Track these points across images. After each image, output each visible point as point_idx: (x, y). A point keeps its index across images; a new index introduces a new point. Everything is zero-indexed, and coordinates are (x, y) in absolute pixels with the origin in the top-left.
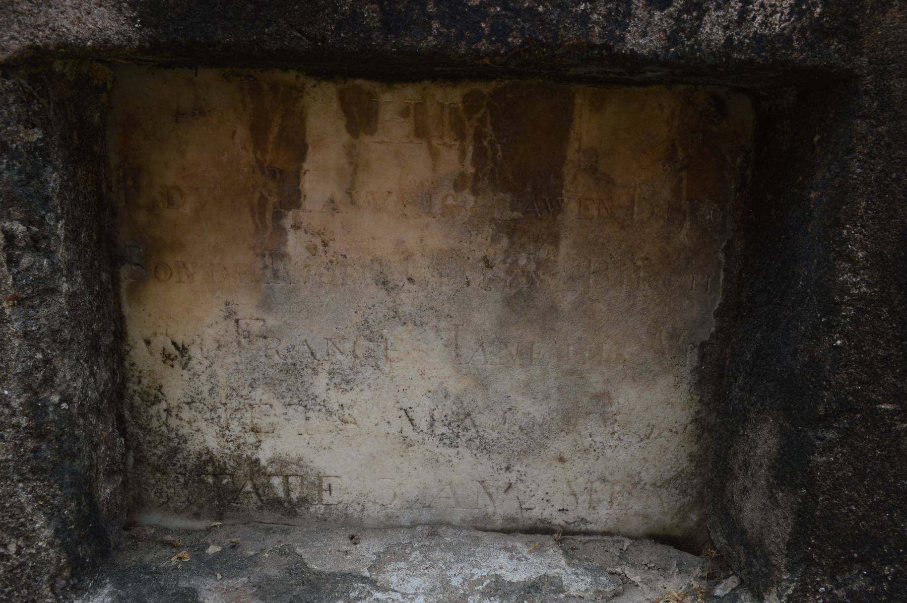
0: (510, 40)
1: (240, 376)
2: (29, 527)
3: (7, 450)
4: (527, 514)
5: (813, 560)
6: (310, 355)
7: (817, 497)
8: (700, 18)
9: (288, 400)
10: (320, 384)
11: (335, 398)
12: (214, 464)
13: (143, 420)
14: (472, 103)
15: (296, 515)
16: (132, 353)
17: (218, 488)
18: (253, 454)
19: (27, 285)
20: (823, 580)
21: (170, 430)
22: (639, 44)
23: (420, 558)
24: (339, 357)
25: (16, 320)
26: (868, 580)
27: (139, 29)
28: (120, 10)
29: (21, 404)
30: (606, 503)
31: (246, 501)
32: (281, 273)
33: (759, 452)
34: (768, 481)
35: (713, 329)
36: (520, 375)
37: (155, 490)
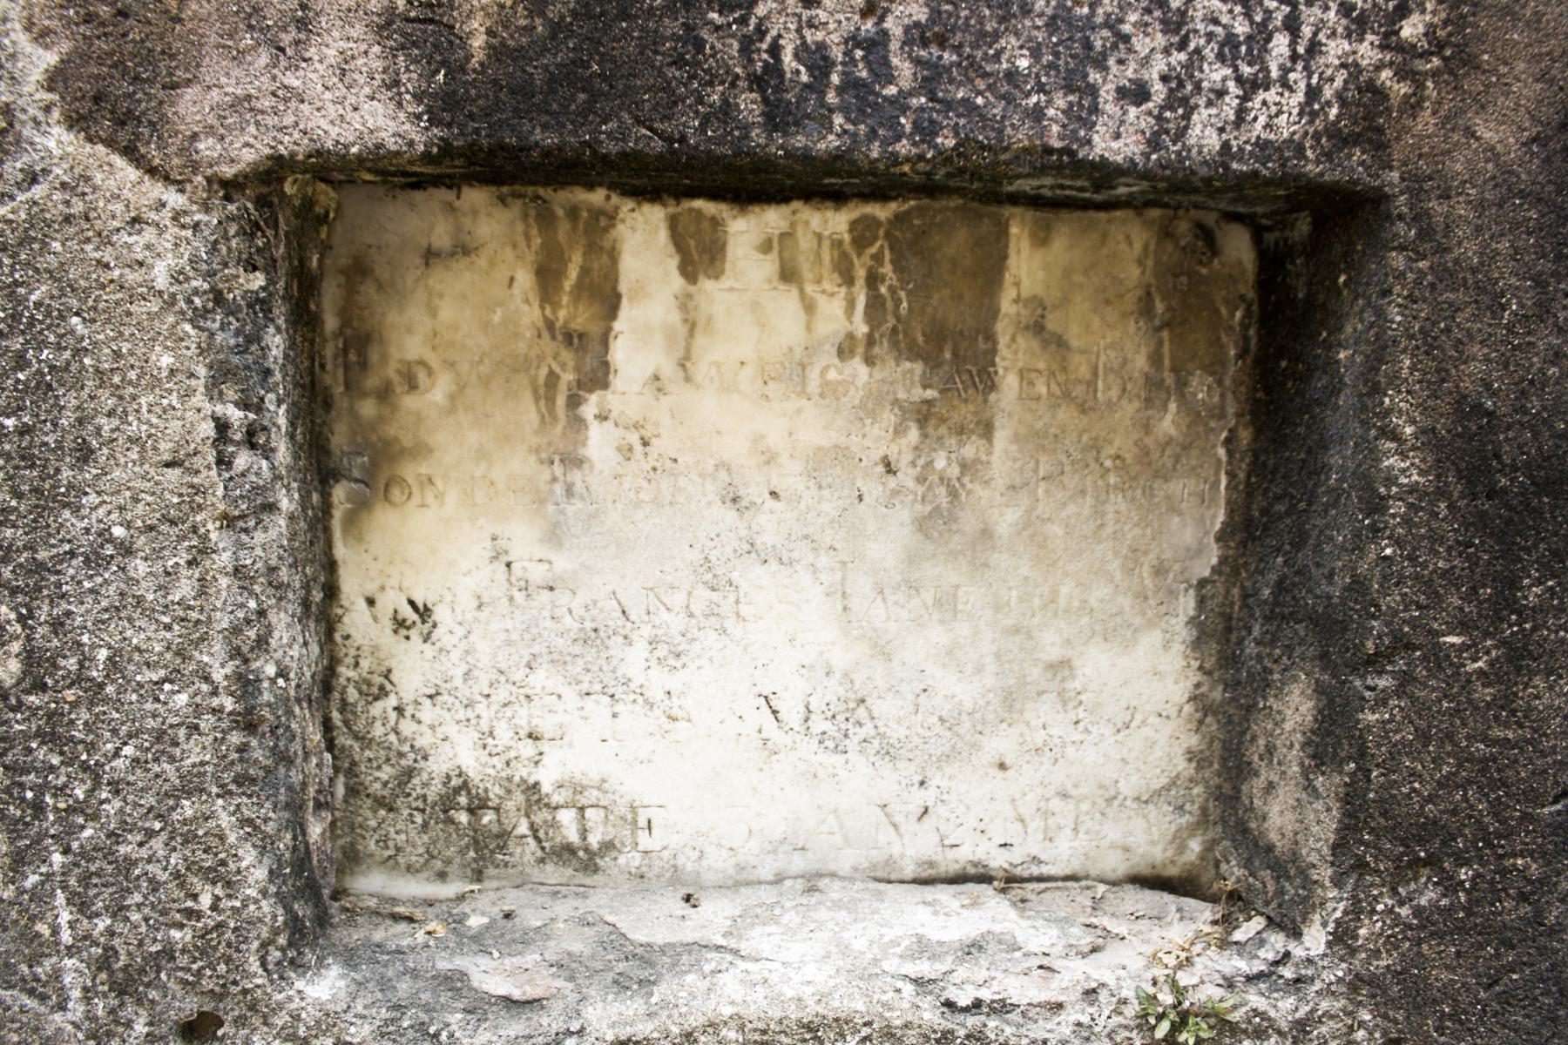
0: (939, 140)
1: (513, 650)
2: (232, 867)
3: (204, 748)
4: (952, 854)
5: (1368, 864)
6: (620, 614)
7: (1370, 771)
8: (1187, 117)
9: (585, 687)
10: (634, 661)
11: (658, 681)
12: (469, 793)
13: (360, 726)
14: (862, 233)
15: (596, 870)
16: (346, 619)
17: (476, 831)
18: (530, 774)
19: (242, 497)
20: (1381, 893)
21: (402, 741)
22: (1111, 149)
23: (798, 920)
24: (665, 616)
25: (224, 550)
26: (1440, 889)
27: (426, 129)
28: (400, 105)
29: (226, 677)
30: (1068, 831)
31: (519, 850)
32: (579, 487)
33: (1288, 726)
34: (1302, 765)
35: (1214, 561)
36: (938, 635)
37: (376, 837)
